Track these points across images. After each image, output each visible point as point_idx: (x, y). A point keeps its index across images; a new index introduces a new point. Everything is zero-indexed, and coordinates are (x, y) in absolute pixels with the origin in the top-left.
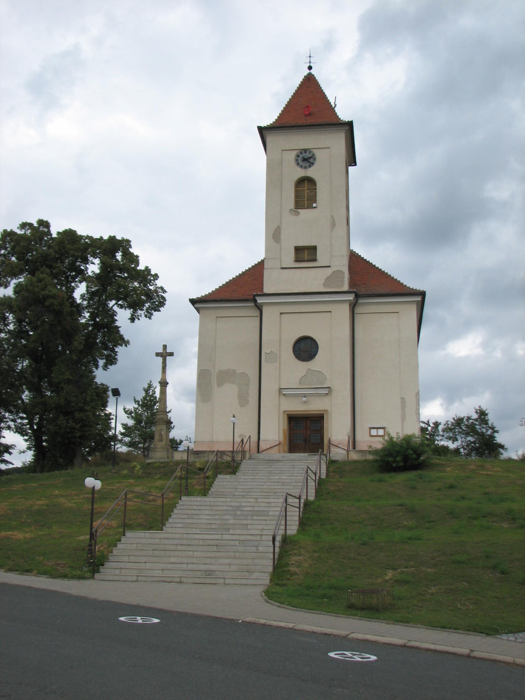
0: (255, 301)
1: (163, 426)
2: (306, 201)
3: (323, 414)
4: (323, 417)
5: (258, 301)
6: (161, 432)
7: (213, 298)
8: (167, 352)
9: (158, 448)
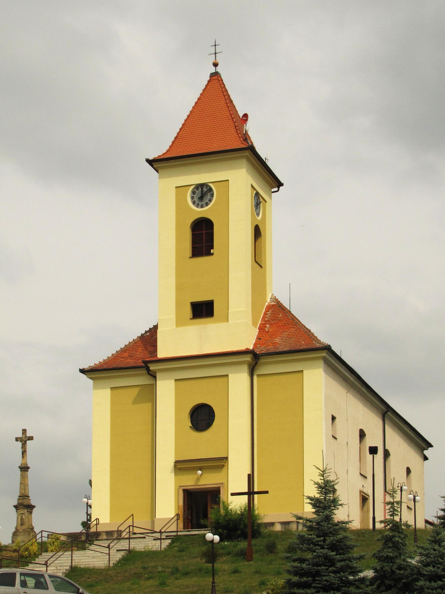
0: (148, 370)
1: (24, 510)
2: (204, 246)
3: (219, 488)
4: (220, 491)
5: (151, 369)
6: (22, 516)
7: (105, 367)
8: (27, 436)
9: (20, 532)
